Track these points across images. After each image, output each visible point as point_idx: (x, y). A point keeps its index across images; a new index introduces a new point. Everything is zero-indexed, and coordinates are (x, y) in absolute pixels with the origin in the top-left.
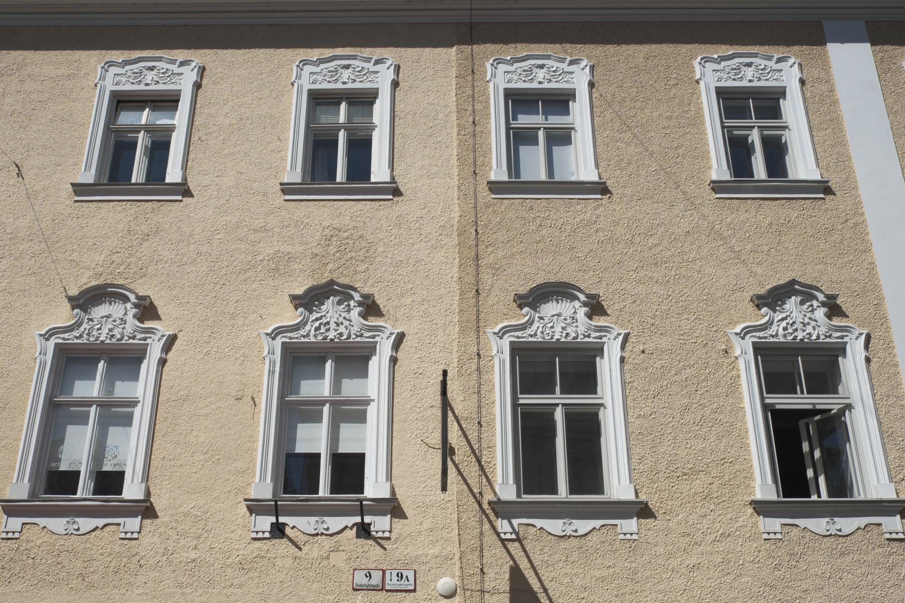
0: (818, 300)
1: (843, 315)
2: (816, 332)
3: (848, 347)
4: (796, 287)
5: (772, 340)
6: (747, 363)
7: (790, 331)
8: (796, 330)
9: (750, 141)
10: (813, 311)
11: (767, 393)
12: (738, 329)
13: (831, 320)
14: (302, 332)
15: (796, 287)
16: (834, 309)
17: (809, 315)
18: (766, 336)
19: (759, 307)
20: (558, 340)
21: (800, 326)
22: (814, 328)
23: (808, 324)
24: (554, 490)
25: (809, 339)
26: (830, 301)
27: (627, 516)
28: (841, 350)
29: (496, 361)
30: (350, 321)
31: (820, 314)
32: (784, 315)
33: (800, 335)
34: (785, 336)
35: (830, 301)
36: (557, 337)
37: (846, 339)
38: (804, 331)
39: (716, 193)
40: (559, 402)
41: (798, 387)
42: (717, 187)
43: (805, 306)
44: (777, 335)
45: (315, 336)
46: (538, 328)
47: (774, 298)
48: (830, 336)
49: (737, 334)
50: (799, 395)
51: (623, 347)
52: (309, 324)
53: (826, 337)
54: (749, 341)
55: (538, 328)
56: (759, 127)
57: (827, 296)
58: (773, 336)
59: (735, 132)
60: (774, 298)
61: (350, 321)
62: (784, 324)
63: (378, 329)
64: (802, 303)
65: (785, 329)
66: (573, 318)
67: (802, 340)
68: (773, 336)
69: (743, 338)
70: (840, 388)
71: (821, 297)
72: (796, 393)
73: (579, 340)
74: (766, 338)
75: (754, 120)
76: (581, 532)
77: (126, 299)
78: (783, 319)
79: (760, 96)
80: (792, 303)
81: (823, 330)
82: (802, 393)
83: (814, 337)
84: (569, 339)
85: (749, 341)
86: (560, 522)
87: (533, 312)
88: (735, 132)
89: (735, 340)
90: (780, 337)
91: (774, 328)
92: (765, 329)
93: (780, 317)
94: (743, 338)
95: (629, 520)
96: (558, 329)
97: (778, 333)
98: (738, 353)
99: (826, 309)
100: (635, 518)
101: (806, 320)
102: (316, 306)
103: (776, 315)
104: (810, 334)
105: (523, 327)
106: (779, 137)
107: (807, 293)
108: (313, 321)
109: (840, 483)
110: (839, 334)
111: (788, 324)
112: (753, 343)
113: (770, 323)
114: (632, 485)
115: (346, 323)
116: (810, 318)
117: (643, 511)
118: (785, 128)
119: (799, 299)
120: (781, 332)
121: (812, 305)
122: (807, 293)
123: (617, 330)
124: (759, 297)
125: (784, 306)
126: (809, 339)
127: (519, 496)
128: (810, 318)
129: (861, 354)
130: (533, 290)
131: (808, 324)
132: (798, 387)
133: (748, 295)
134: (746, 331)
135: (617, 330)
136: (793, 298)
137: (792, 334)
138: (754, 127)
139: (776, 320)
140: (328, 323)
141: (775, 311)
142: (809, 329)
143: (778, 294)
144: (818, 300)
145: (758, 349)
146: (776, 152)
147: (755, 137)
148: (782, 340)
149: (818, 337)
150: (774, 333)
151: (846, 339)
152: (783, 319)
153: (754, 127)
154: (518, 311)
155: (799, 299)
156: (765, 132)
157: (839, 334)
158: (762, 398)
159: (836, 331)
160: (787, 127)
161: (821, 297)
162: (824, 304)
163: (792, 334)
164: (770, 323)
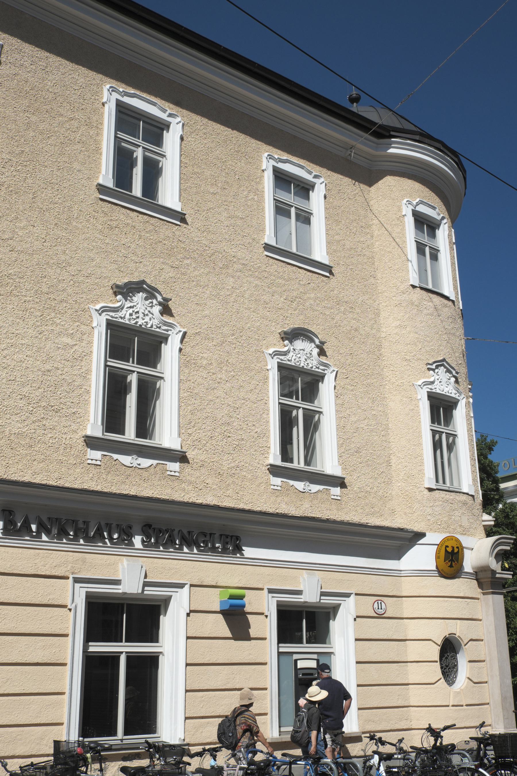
0: (157, 300)
1: (171, 315)
2: (151, 322)
3: (326, 377)
4: (145, 286)
5: (120, 320)
6: (100, 334)
7: (134, 317)
8: (138, 317)
9: (135, 156)
10: (152, 307)
11: (109, 358)
12: (98, 307)
13: (162, 316)
14: (120, 314)
15: (145, 286)
16: (166, 310)
17: (149, 309)
18: (117, 317)
19: (116, 294)
20: (303, 367)
21: (141, 315)
22: (150, 319)
23: (147, 315)
24: (122, 432)
25: (145, 326)
26: (165, 302)
27: (335, 485)
28: (165, 339)
29: (96, 331)
30: (153, 314)
31: (157, 309)
32: (132, 304)
33: (140, 322)
34: (129, 320)
35: (165, 302)
36: (302, 365)
37: (169, 333)
38: (143, 319)
39: (100, 193)
40: (134, 372)
41: (131, 359)
42: (102, 189)
43: (148, 302)
44: (124, 318)
45: (129, 320)
46: (293, 356)
47: (127, 290)
48: (160, 328)
49: (96, 310)
50: (131, 364)
51: (182, 341)
52: (125, 309)
53: (157, 327)
54: (105, 317)
55: (293, 356)
56: (143, 148)
57: (164, 299)
58: (121, 318)
59: (123, 144)
60: (127, 290)
61: (153, 314)
62: (131, 311)
63: (326, 365)
64: (146, 299)
65: (131, 315)
66: (311, 354)
67: (140, 325)
68: (121, 318)
69: (100, 314)
70: (159, 366)
71: (160, 298)
72: (128, 362)
73: (313, 369)
74: (116, 318)
75: (140, 141)
76: (313, 491)
77: (312, 341)
78: (130, 307)
79: (149, 121)
80: (139, 297)
81: (155, 322)
82: (133, 363)
83: (149, 326)
84: (309, 367)
85: (105, 317)
86: (130, 458)
87: (124, 301)
88: (123, 144)
89: (95, 315)
90: (126, 319)
91: (124, 312)
92: (117, 311)
93: (129, 306)
94: (100, 314)
95: (336, 488)
96: (303, 359)
97: (125, 317)
98: (94, 324)
99: (161, 308)
100: (339, 488)
101: (146, 312)
102: (131, 297)
103: (126, 303)
104: (146, 322)
105: (285, 354)
106: (158, 162)
107: (151, 293)
108: (128, 308)
109: (144, 428)
110: (166, 328)
111: (133, 311)
112: (107, 319)
113: (121, 308)
114: (180, 439)
115: (150, 316)
116: (149, 312)
117: (182, 458)
118: (163, 156)
119: (145, 295)
120: (128, 316)
121: (152, 303)
122: (151, 293)
123: (179, 328)
124: (117, 286)
125: (134, 298)
126: (145, 326)
127: (103, 434)
128: (149, 312)
129: (178, 345)
130: (126, 284)
131: (147, 315)
132: (131, 359)
133: (111, 283)
134: (104, 310)
135: (179, 328)
136: (141, 293)
137: (135, 319)
138: (140, 146)
139: (126, 307)
140: (137, 312)
141: (126, 301)
142: (147, 319)
143: (131, 288)
144: (157, 300)
145: (110, 325)
146: (153, 172)
147: (139, 154)
148: (127, 322)
149: (152, 327)
150: (123, 316)
151: (169, 333)
152: (130, 307)
153: (140, 146)
154: (113, 297)
155: (145, 295)
156: (147, 153)
157: (166, 328)
158: (106, 361)
159: (165, 325)
160: (165, 156)
161: (160, 298)
162: (160, 304)
163: (135, 319)
164: (288, 351)
